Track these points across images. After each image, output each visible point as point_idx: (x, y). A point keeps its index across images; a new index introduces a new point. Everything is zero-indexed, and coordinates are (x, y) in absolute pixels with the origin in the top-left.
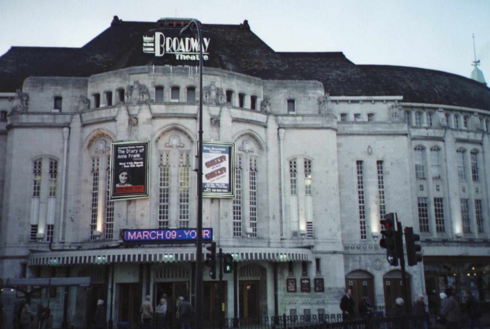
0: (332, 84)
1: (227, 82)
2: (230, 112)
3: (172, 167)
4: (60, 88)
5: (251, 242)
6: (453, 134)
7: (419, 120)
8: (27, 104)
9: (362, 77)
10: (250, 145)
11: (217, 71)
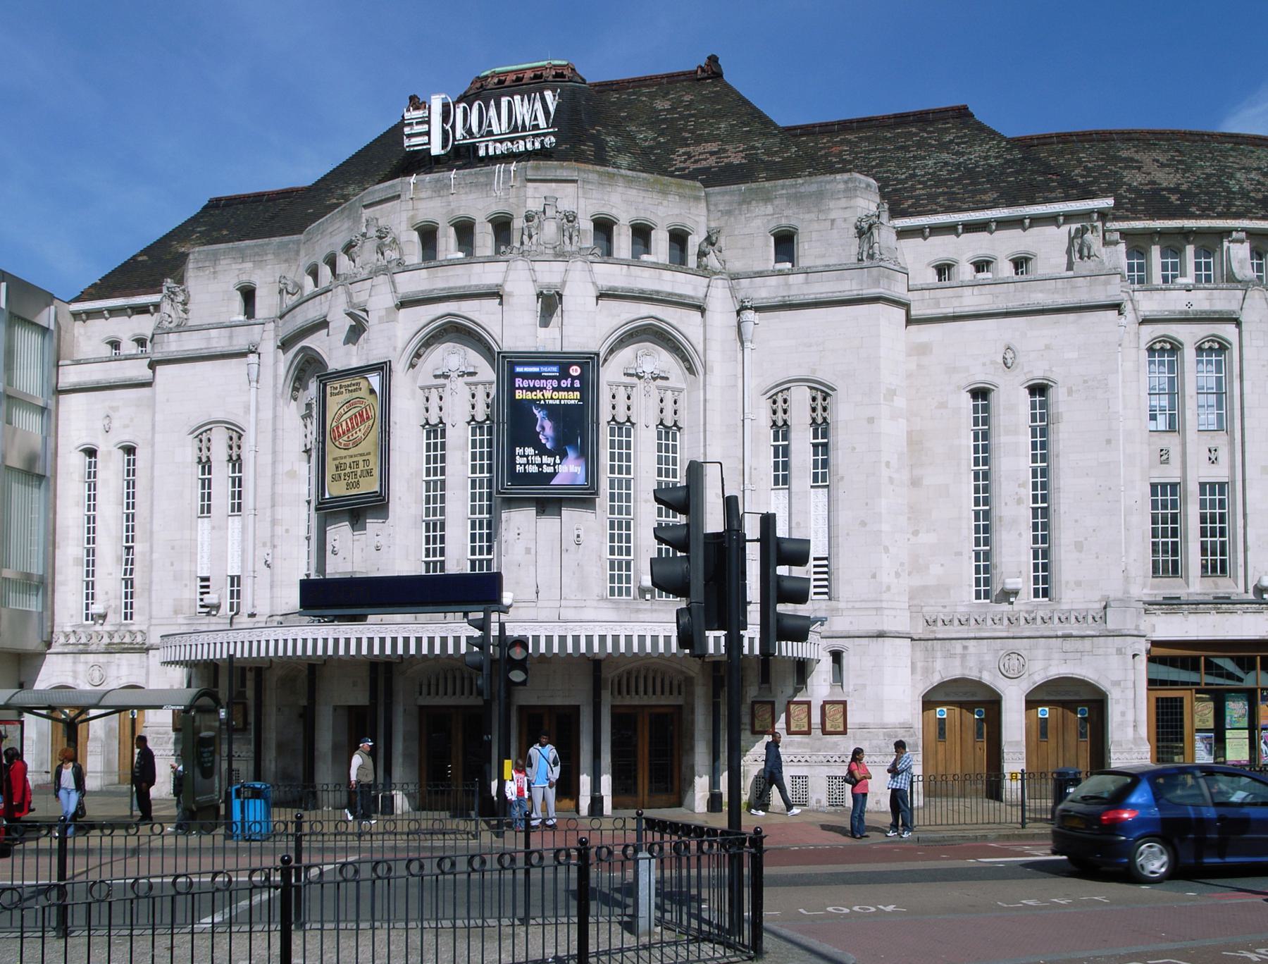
1: (595, 194)
2: (591, 271)
4: (249, 265)
5: (652, 611)
8: (185, 311)
9: (1007, 161)
10: (658, 359)
11: (567, 168)
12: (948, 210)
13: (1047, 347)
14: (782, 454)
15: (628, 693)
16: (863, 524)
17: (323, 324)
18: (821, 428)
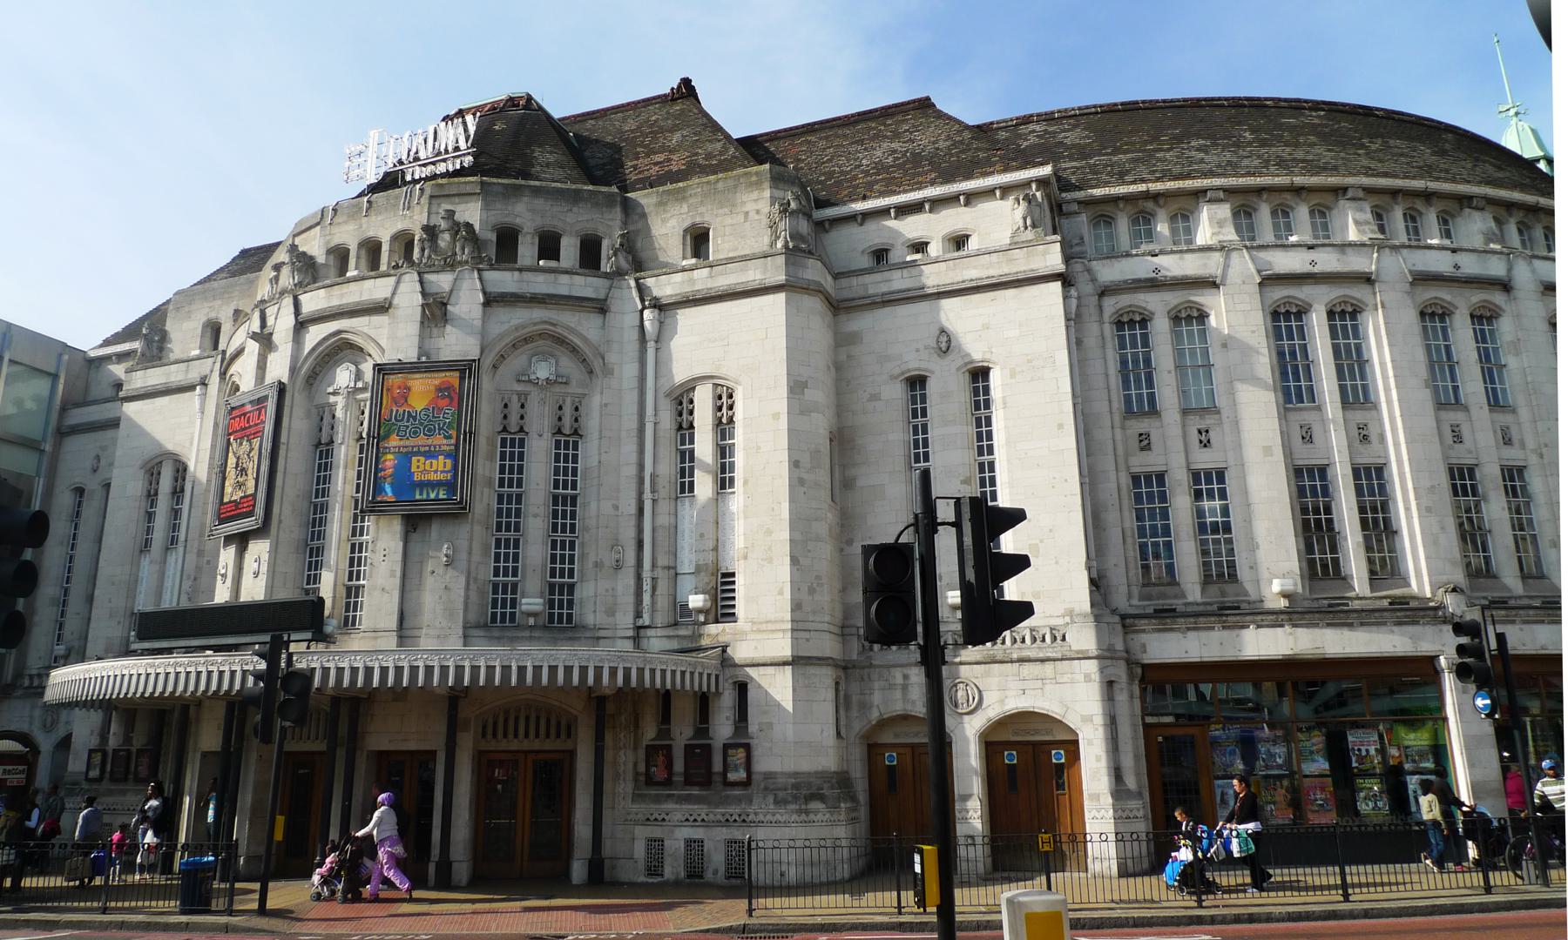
0: (1447, 146)
1: (498, 206)
3: (533, 435)
7: (1414, 230)
12: (882, 194)
13: (986, 327)
15: (505, 735)
18: (724, 428)
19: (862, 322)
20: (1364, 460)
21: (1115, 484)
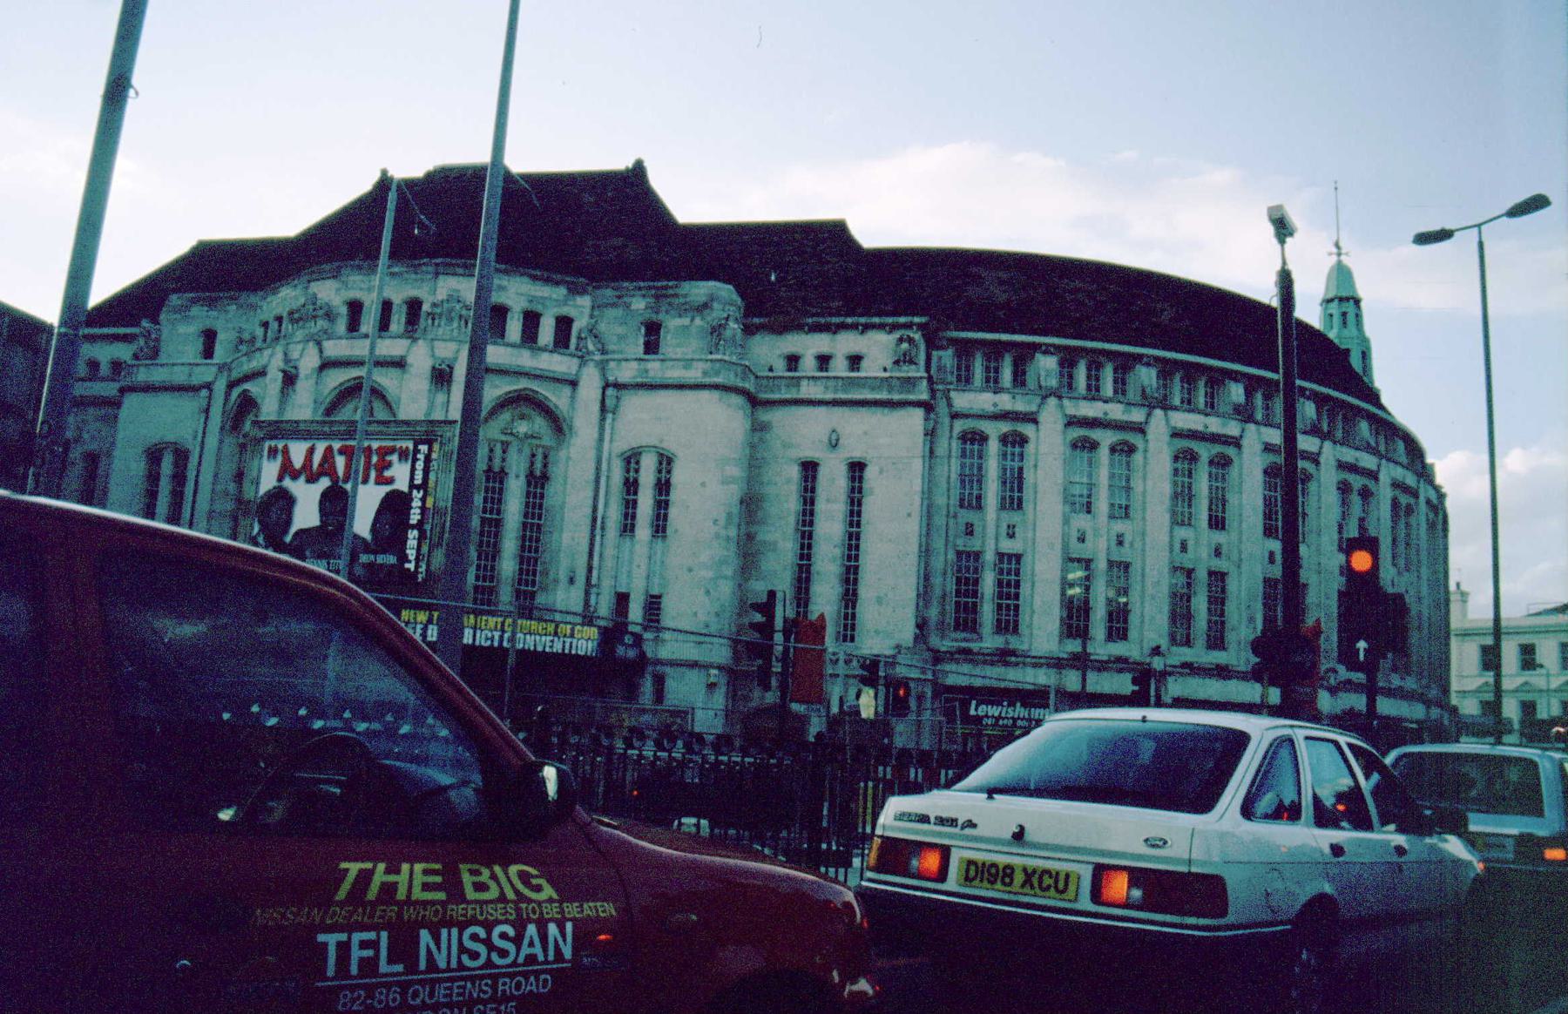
3: (512, 475)
6: (1259, 433)
14: (630, 506)
16: (690, 570)
17: (261, 373)
18: (663, 487)
19: (775, 416)
20: (1115, 558)
21: (942, 559)
